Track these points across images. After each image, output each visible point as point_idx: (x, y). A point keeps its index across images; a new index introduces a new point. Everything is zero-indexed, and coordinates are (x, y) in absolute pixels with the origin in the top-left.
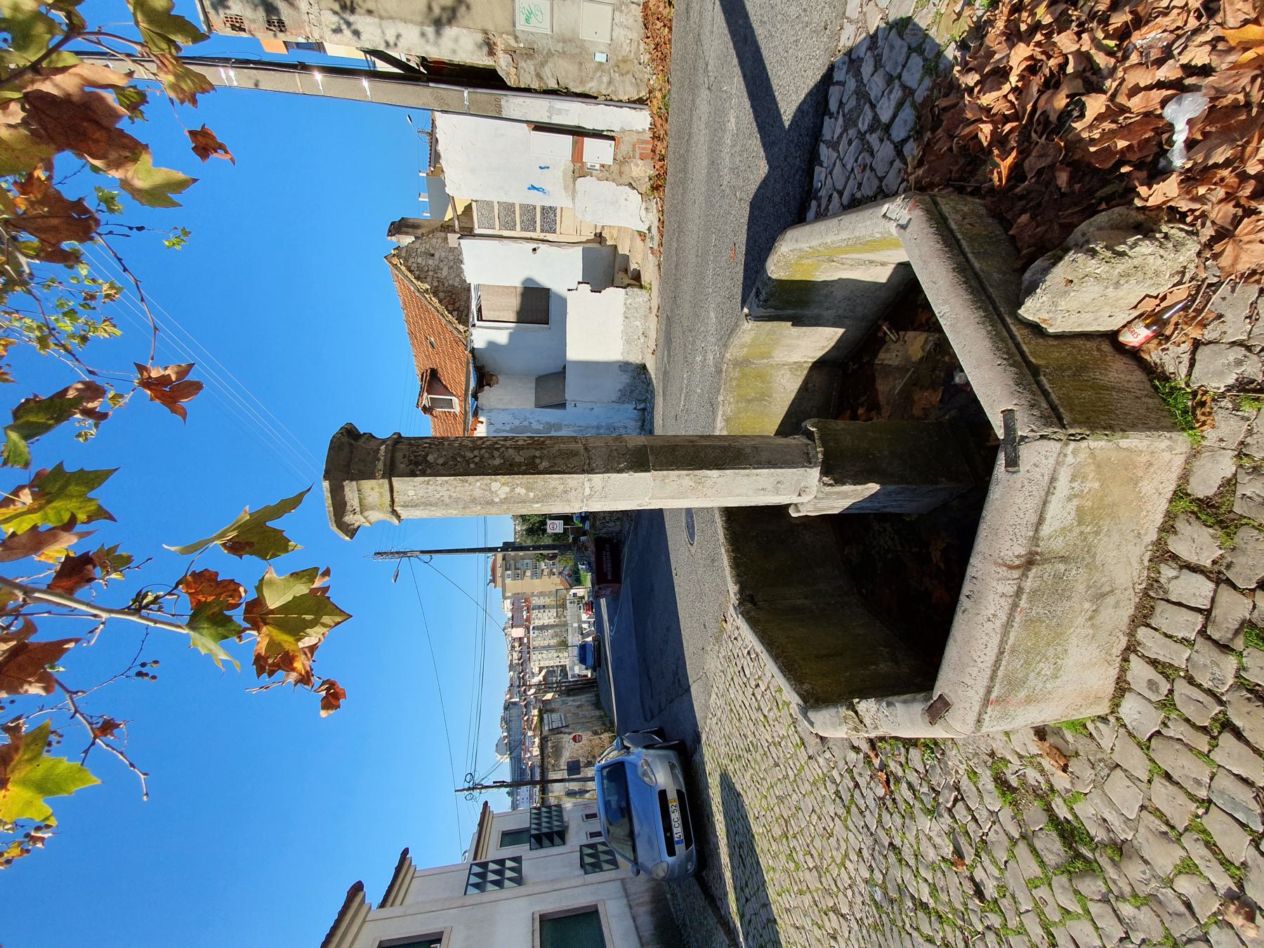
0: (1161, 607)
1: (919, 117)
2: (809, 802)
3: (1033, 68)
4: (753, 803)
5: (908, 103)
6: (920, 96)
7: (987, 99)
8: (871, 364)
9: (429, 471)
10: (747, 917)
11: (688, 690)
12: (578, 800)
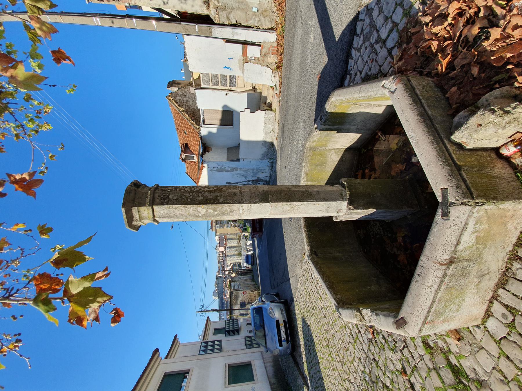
0: (511, 281)
1: (400, 37)
2: (338, 335)
3: (461, 13)
4: (314, 330)
5: (395, 30)
6: (401, 27)
7: (436, 29)
8: (372, 150)
9: (170, 202)
10: (311, 375)
11: (289, 280)
12: (244, 317)
